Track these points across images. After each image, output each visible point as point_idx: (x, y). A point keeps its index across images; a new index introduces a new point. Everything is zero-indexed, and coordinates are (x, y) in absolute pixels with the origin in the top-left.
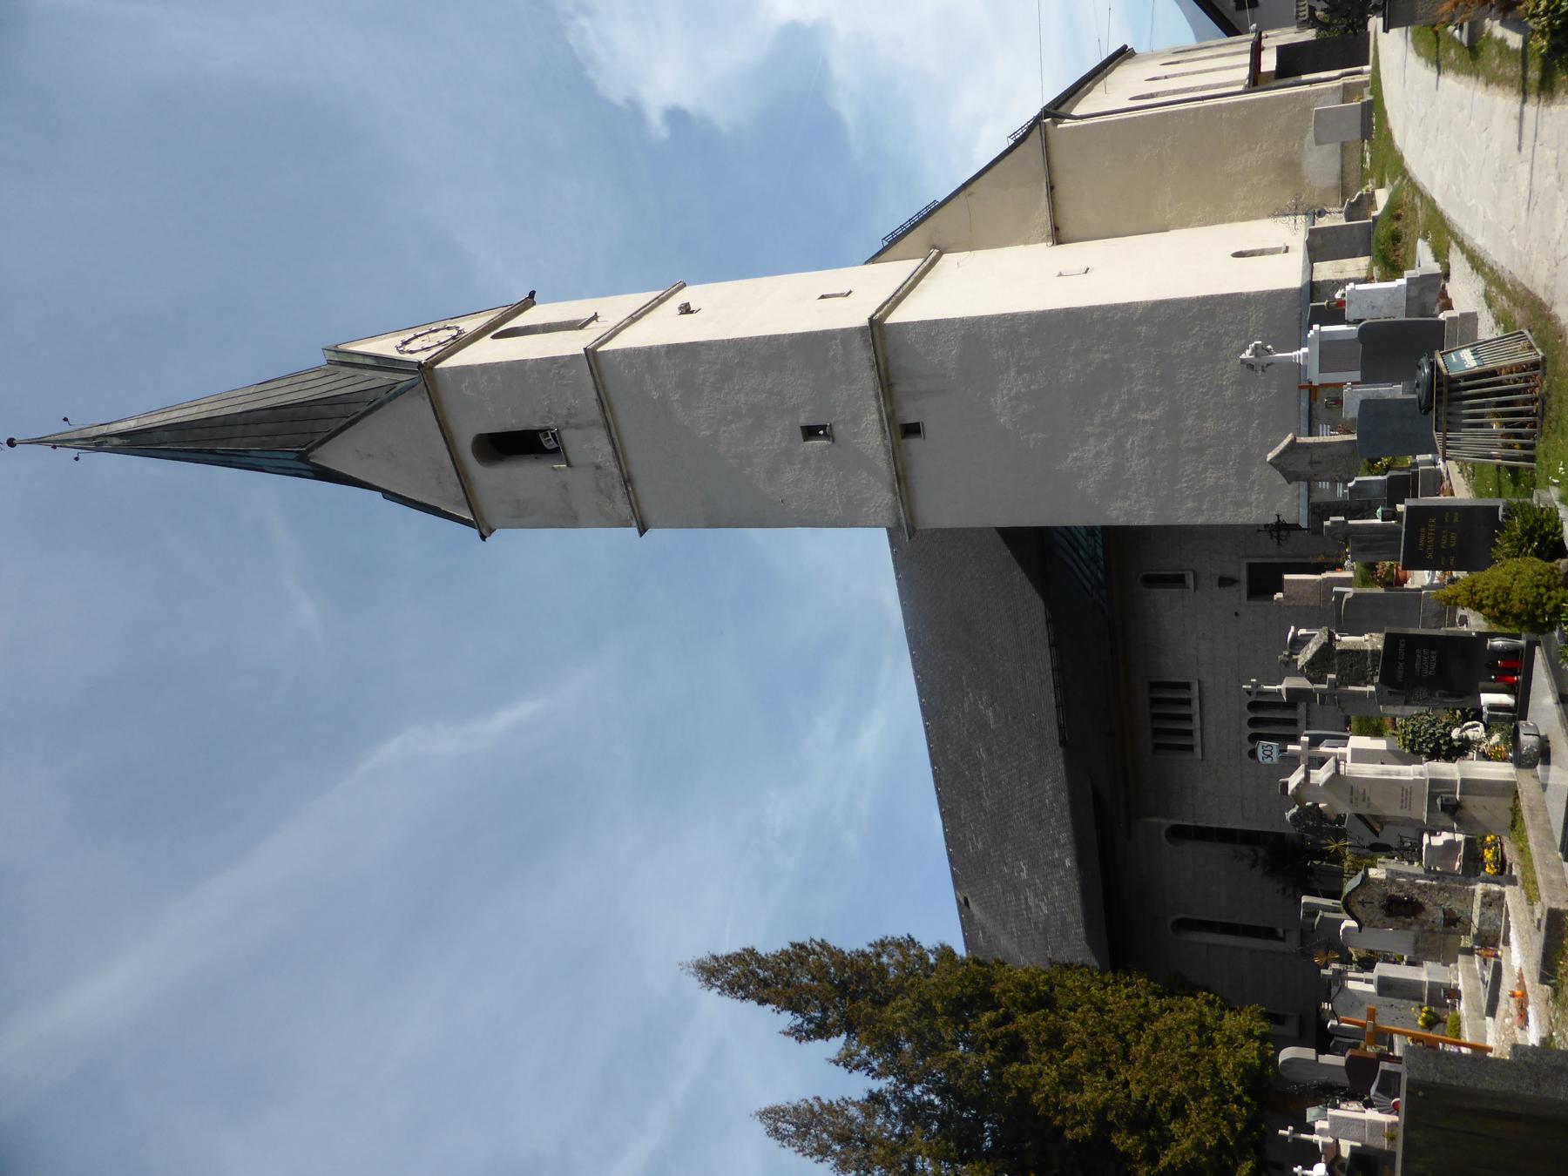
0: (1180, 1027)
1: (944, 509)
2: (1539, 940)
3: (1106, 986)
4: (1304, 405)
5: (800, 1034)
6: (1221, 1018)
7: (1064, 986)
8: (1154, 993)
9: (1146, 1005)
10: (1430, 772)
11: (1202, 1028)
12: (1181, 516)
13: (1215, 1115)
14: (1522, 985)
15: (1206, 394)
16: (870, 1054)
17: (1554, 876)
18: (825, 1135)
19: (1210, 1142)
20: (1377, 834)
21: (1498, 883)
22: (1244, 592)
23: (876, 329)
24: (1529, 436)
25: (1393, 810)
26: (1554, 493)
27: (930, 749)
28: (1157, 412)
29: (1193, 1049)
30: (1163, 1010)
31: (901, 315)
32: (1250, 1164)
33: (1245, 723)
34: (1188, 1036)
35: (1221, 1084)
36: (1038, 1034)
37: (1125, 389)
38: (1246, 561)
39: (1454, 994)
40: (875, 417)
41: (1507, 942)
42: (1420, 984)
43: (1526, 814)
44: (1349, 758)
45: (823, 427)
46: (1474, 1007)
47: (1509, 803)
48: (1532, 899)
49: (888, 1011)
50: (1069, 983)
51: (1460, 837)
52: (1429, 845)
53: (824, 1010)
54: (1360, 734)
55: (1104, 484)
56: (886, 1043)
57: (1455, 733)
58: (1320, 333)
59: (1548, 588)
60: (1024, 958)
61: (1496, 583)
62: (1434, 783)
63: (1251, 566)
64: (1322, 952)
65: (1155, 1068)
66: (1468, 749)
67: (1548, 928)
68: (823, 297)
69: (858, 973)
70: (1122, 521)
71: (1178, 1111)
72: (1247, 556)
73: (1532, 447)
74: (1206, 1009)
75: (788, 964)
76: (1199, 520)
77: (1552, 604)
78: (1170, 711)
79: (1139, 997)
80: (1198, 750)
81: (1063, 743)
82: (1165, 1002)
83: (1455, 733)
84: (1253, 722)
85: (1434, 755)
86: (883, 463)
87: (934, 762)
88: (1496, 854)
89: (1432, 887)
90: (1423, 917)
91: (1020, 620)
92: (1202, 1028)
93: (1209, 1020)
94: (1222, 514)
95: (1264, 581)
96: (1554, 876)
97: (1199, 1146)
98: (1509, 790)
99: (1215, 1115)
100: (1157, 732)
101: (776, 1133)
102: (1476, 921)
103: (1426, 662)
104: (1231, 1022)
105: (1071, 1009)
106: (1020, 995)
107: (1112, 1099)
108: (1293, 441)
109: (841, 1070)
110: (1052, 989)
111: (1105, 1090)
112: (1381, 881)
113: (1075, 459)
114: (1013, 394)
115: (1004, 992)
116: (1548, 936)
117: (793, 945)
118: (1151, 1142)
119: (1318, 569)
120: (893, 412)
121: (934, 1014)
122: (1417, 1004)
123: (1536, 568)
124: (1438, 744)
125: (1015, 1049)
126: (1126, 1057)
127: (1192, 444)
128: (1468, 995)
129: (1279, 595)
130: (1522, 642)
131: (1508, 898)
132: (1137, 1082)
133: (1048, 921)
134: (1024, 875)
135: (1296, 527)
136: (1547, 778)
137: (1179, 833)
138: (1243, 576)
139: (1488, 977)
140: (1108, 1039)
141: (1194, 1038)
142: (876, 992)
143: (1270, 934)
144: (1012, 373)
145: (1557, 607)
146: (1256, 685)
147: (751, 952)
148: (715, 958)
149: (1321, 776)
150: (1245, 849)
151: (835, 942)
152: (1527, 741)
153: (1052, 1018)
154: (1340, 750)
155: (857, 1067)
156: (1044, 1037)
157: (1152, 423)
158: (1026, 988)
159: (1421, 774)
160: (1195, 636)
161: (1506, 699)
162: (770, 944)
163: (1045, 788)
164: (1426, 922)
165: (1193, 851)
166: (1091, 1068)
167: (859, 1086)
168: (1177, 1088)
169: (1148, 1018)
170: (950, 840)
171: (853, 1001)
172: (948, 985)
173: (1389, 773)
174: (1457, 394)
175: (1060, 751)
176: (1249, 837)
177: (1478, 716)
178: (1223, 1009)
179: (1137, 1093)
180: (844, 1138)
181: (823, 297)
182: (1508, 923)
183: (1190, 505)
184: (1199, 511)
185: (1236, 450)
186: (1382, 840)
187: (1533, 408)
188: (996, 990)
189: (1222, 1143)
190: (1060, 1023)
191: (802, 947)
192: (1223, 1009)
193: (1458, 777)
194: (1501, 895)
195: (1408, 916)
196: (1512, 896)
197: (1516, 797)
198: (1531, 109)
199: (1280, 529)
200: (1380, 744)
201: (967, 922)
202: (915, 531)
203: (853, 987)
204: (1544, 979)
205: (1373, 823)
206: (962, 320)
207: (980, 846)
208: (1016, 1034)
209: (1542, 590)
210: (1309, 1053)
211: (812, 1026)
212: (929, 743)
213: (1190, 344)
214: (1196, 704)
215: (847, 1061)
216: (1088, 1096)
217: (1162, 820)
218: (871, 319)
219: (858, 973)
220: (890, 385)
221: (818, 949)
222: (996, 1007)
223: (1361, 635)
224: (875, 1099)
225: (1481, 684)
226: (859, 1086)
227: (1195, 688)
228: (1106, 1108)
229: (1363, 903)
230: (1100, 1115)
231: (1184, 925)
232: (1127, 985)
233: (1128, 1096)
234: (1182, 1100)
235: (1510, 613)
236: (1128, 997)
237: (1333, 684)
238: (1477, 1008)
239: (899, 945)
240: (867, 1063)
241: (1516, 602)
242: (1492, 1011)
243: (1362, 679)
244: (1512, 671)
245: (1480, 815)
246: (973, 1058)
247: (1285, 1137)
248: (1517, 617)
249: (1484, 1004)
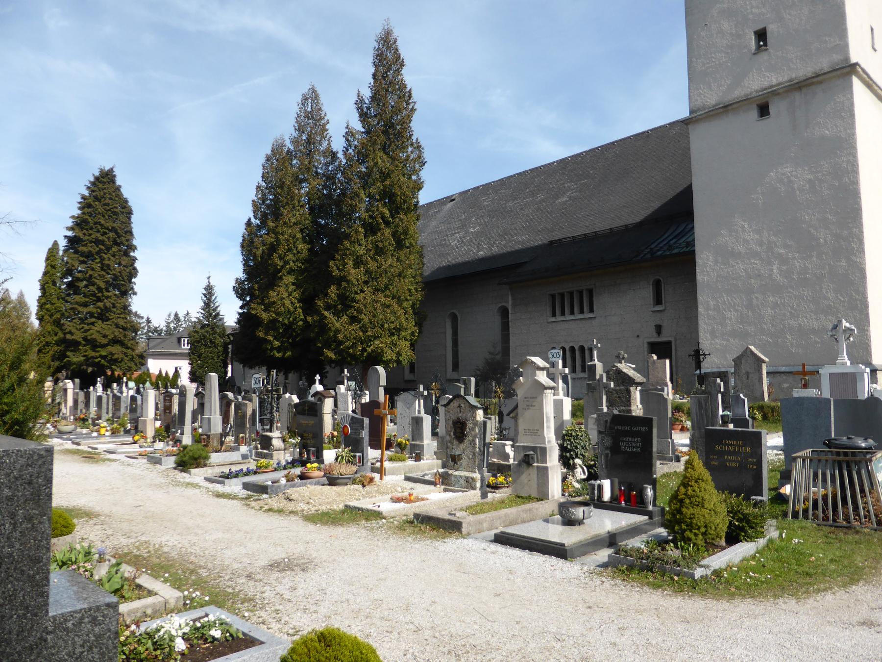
0: (397, 318)
1: (702, 144)
2: (443, 514)
3: (414, 277)
4: (783, 369)
5: (360, 102)
6: (406, 340)
7: (410, 254)
8: (414, 304)
9: (407, 300)
10: (551, 448)
11: (399, 330)
12: (702, 297)
13: (354, 338)
14: (418, 499)
15: (792, 308)
16: (356, 147)
17: (485, 525)
18: (309, 129)
19: (340, 337)
20: (508, 414)
21: (482, 486)
22: (652, 340)
23: (848, 69)
24: (816, 517)
25: (522, 425)
26: (774, 534)
27: (540, 167)
28: (778, 278)
29: (386, 325)
30: (405, 309)
31: (857, 84)
32: (333, 357)
33: (572, 344)
34: (393, 323)
35: (371, 341)
36: (381, 241)
37: (797, 255)
38: (672, 339)
39: (418, 458)
40: (774, 82)
41: (445, 490)
42: (422, 439)
43: (528, 506)
44: (556, 397)
45: (765, 44)
46: (411, 470)
47: (534, 494)
48: (472, 509)
49: (380, 154)
50: (412, 257)
51: (511, 461)
52: (505, 445)
53: (375, 116)
54: (573, 406)
55: (723, 249)
56: (362, 155)
57: (578, 461)
58: (863, 374)
59: (704, 534)
60: (424, 234)
61: (707, 497)
62: (544, 450)
63: (669, 343)
64: (439, 387)
65: (373, 306)
66: (568, 468)
67: (449, 521)
68: (872, 30)
69: (399, 133)
70: (699, 261)
71: (354, 320)
72: (675, 341)
73: (806, 517)
74: (409, 332)
75: (399, 89)
76: (701, 309)
77: (692, 536)
78: (578, 302)
79: (410, 296)
80: (553, 319)
81: (551, 243)
82: (410, 311)
83: (578, 461)
84: (572, 349)
85: (563, 449)
86: (738, 93)
87: (532, 170)
88: (502, 483)
89: (475, 448)
90: (455, 442)
91: (625, 206)
92: (399, 330)
93: (403, 333)
94: (705, 323)
95: (662, 349)
96: (485, 525)
97: (338, 331)
98: (543, 496)
99: (354, 338)
100: (562, 296)
101: (305, 99)
102: (457, 473)
103: (633, 445)
104: (404, 346)
105: (398, 259)
106: (401, 229)
107: (353, 284)
108: (763, 361)
109: (345, 130)
110: (407, 248)
111: (358, 280)
112: (475, 417)
113: (743, 227)
114: (793, 179)
115: (401, 220)
116: (444, 521)
117: (410, 91)
118: (335, 306)
119: (671, 380)
120: (778, 94)
121: (383, 181)
122: (410, 438)
123: (721, 526)
124: (570, 451)
125: (371, 229)
126: (377, 290)
127: (755, 302)
128: (417, 466)
129: (655, 357)
130: (651, 508)
131: (472, 492)
132: (365, 297)
133: (448, 246)
134: (471, 230)
135: (698, 366)
136: (553, 523)
137: (504, 313)
138: (663, 339)
139: (427, 478)
140: (384, 281)
141: (392, 326)
142: (390, 145)
143: (456, 366)
144: (809, 177)
145: (690, 540)
146: (596, 346)
147: (402, 65)
148: (395, 42)
149: (542, 377)
150: (499, 348)
151: (416, 117)
152: (579, 512)
153: (391, 248)
154: (561, 392)
155: (347, 140)
156: (380, 245)
157: (771, 275)
158: (406, 233)
159: (549, 442)
160: (622, 315)
161: (607, 496)
162: (409, 77)
163: (522, 235)
164: (452, 444)
165: (496, 321)
166: (368, 272)
167: (338, 144)
168: (365, 318)
169: (400, 302)
170: (487, 187)
171: (383, 132)
172: (400, 187)
173: (548, 421)
174: (844, 466)
175: (546, 242)
176: (506, 351)
177: (592, 476)
178: (411, 340)
179: (358, 297)
180: (309, 141)
181: (872, 30)
182: (458, 491)
183: (712, 303)
184: (708, 309)
185: (751, 329)
186: (505, 418)
187: (841, 519)
188: (402, 215)
189: (341, 343)
190: (389, 253)
191: (410, 97)
192: (411, 340)
193: (549, 464)
194: (474, 488)
195: (454, 434)
196: (474, 495)
197: (539, 499)
198: (246, 369)
199: (697, 356)
200: (567, 416)
201: (441, 202)
202: (687, 124)
203: (391, 131)
204: (417, 516)
205: (515, 412)
206: (854, 134)
207: (486, 203)
208: (380, 229)
209: (703, 530)
210: (383, 381)
211: (365, 110)
212: (544, 166)
213: (831, 295)
214: (581, 316)
215: (349, 134)
216: (353, 271)
217: (510, 302)
218: (857, 64)
219: (399, 133)
220: (800, 88)
221: (410, 107)
222: (392, 216)
223: (641, 403)
224: (334, 155)
225: (616, 480)
226: (338, 144)
227: (591, 315)
228: (348, 282)
229: (460, 406)
230: (344, 279)
231: (454, 319)
232: (416, 289)
233: (357, 293)
234: (359, 321)
235: (681, 506)
236: (409, 290)
237: (606, 386)
238: (410, 471)
239: (420, 157)
240: (350, 146)
241: (691, 511)
242: (408, 479)
243: (610, 404)
244: (629, 499)
245: (524, 478)
246: (363, 206)
247: (343, 372)
248: (679, 511)
249: (411, 475)
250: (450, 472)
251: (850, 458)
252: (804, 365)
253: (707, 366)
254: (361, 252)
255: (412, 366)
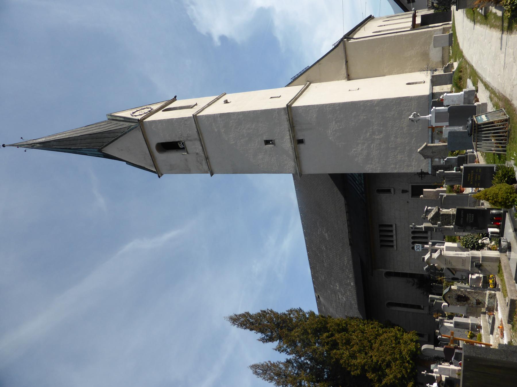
0: (389, 338)
1: (311, 168)
2: (507, 309)
3: (365, 324)
4: (430, 133)
5: (264, 340)
6: (403, 335)
7: (351, 325)
8: (381, 327)
9: (378, 331)
10: (472, 254)
11: (396, 338)
12: (390, 170)
13: (401, 367)
14: (502, 324)
15: (398, 130)
16: (287, 347)
17: (513, 288)
18: (272, 374)
19: (399, 376)
20: (454, 274)
21: (494, 291)
22: (410, 195)
23: (289, 108)
24: (504, 143)
25: (459, 267)
26: (512, 162)
27: (307, 246)
28: (382, 136)
29: (393, 345)
30: (383, 333)
31: (297, 104)
32: (412, 383)
33: (410, 238)
34: (392, 341)
35: (403, 357)
36: (342, 340)
37: (371, 128)
38: (411, 185)
39: (480, 327)
40: (289, 137)
41: (497, 310)
42: (468, 324)
43: (503, 268)
44: (445, 250)
45: (272, 141)
46: (486, 331)
47: (498, 264)
48: (505, 296)
49: (293, 333)
50: (353, 324)
51: (481, 276)
52: (471, 278)
53: (272, 333)
54: (448, 241)
55: (364, 159)
56: (292, 343)
57: (480, 241)
58: (435, 109)
59: (510, 194)
60: (337, 315)
62: (473, 258)
63: (412, 186)
64: (436, 313)
65: (381, 352)
66: (484, 246)
67: (510, 305)
68: (271, 98)
69: (283, 320)
70: (370, 171)
71: (388, 366)
72: (411, 183)
73: (505, 147)
74: (398, 332)
75: (260, 317)
76: (395, 171)
77: (512, 199)
78: (386, 234)
79: (375, 328)
80: (395, 247)
81: (351, 244)
82: (384, 330)
83: (480, 241)
84: (413, 238)
85: (473, 248)
86: (291, 152)
87: (308, 251)
88: (493, 281)
89: (472, 292)
90: (469, 302)
91: (336, 204)
92: (396, 338)
93: (399, 336)
94: (403, 169)
95: (417, 191)
96: (513, 288)
97: (395, 377)
98: (498, 260)
99: (401, 367)
100: (382, 241)
101: (256, 373)
102: (487, 303)
103: (470, 218)
104: (406, 336)
105: (353, 332)
106: (336, 328)
107: (367, 362)
108: (426, 145)
109: (277, 352)
110: (347, 326)
111: (364, 359)
112: (455, 290)
113: (355, 151)
114: (334, 130)
115: (331, 326)
116: (511, 308)
117: (261, 311)
118: (379, 376)
119: (435, 187)
120: (294, 135)
121: (308, 334)
122: (467, 330)
123: (507, 187)
124: (474, 245)
125: (335, 345)
126: (371, 348)
127: (393, 146)
128: (484, 328)
129: (422, 196)
130: (502, 211)
131: (497, 295)
132: (375, 356)
133: (346, 303)
134: (338, 288)
135: (427, 173)
136: (510, 256)
137: (389, 274)
138: (410, 189)
139: (491, 322)
140: (365, 342)
141: (394, 341)
142: (289, 327)
143: (419, 307)
144: (334, 123)
145: (513, 200)
146: (414, 226)
147: (248, 313)
148: (236, 315)
149: (435, 255)
150: (410, 279)
151: (275, 310)
152: (504, 244)
153: (347, 335)
154: (442, 247)
155: (283, 351)
156: (344, 341)
157: (380, 139)
158: (338, 325)
159: (469, 255)
160: (394, 209)
161: (496, 230)
162: (254, 311)
163: (345, 259)
164: (470, 303)
165: (393, 280)
166: (360, 351)
167: (283, 357)
168: (388, 358)
169: (379, 335)
170: (313, 276)
171: (281, 329)
172: (313, 324)
173: (458, 254)
174: (480, 130)
175: (350, 247)
176: (412, 276)
177: (487, 236)
178: (403, 332)
179: (375, 360)
180: (278, 375)
181: (271, 98)
182: (497, 304)
183: (392, 166)
184: (395, 168)
185: (408, 148)
186: (456, 276)
187: (505, 134)
188: (328, 326)
189: (403, 376)
190: (350, 337)
191: (265, 312)
192: (403, 332)
193: (481, 256)
194: (495, 295)
195: (464, 301)
196: (499, 295)
197: (500, 262)
198: (505, 36)
199: (422, 174)
200: (455, 245)
202: (302, 175)
203: (281, 325)
204: (509, 322)
205: (453, 271)
206: (317, 105)
207: (323, 278)
208: (335, 340)
209: (509, 194)
210: (432, 347)
211: (268, 338)
212: (306, 244)
213: (392, 113)
214: (394, 232)
215: (279, 349)
216: (359, 361)
217: (383, 270)
218: (287, 105)
219: (283, 320)
220: (293, 127)
221: (270, 312)
222: (328, 332)
223: (449, 209)
224: (289, 362)
225: (488, 225)
226: (283, 357)
227: (394, 226)
228: (365, 365)
229: (449, 297)
230: (363, 367)
231: (391, 304)
232: (372, 324)
234: (390, 362)
235: (498, 202)
236: (372, 328)
237: (439, 225)
238: (487, 332)
239: (296, 311)
240: (286, 350)
241: (500, 198)
242: (492, 333)
243: (449, 224)
244: (499, 221)
245: (488, 268)
246: (321, 348)
247: (424, 374)
248: (500, 203)
249: (489, 330)
250: (486, 306)
251: (476, 128)
252: (429, 128)
253: (428, 169)
254: (348, 353)
255: (418, 334)
